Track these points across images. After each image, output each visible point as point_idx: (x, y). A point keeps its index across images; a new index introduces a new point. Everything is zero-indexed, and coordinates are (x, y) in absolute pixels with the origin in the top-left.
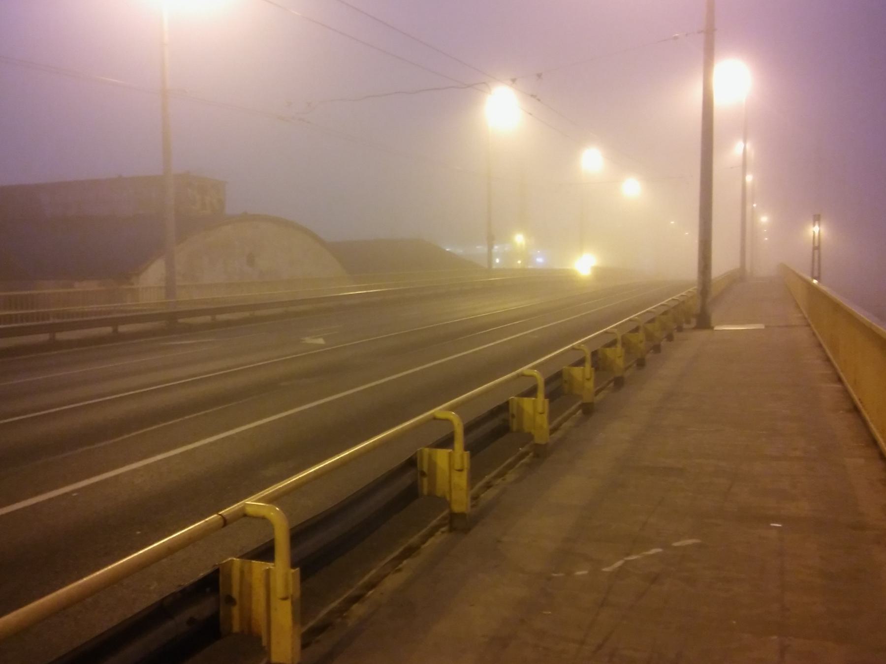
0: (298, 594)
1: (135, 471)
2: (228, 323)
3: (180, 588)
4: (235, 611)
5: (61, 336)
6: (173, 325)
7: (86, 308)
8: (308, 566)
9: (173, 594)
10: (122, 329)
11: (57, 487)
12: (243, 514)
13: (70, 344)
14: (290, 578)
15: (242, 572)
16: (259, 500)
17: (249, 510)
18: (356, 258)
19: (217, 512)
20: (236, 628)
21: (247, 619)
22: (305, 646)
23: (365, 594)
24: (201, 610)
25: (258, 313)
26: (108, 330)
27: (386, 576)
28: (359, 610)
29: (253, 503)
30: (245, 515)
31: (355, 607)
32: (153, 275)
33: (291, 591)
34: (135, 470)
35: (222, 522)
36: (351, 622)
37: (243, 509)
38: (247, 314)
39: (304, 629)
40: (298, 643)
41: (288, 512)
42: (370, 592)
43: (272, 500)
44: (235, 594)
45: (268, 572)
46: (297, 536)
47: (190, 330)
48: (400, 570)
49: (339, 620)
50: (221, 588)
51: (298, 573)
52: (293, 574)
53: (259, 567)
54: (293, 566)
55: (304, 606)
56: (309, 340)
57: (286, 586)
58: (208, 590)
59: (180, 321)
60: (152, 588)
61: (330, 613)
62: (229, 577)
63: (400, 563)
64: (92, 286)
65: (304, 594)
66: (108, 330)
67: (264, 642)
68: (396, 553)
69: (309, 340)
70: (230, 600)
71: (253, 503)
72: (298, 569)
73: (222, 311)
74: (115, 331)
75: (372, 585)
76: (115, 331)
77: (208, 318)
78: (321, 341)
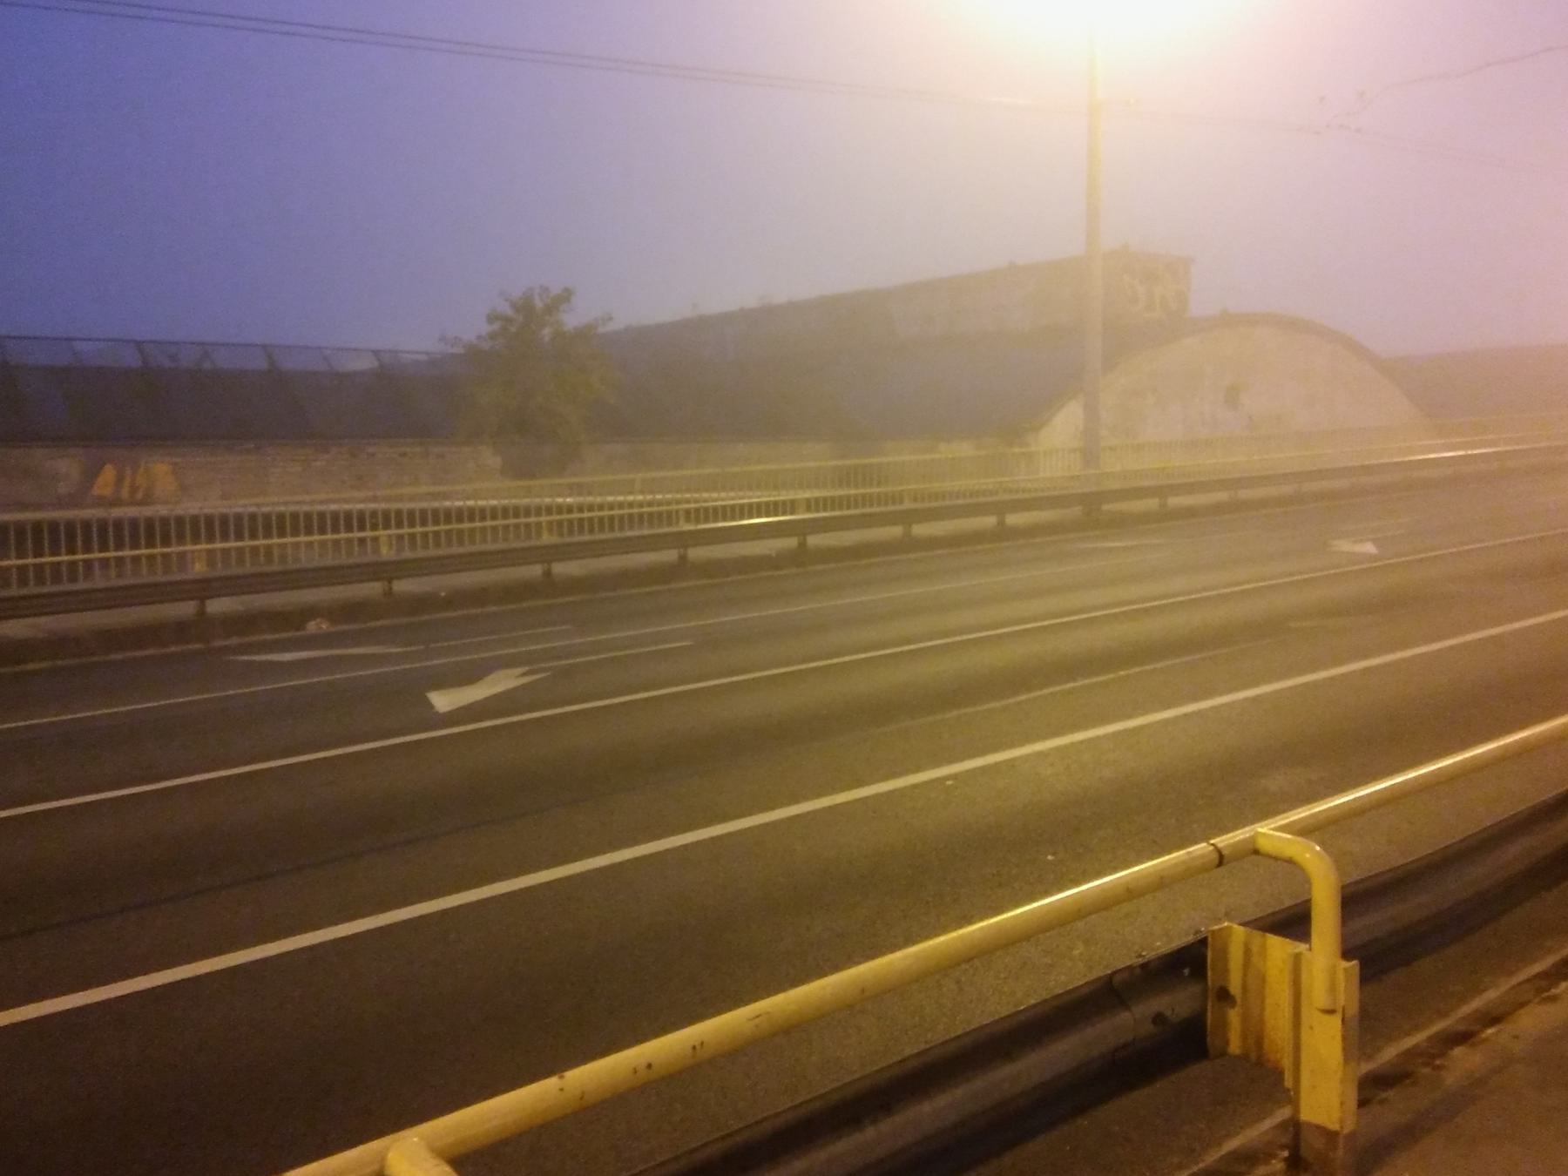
0: (1353, 1009)
1: (1046, 754)
2: (1191, 513)
3: (1141, 961)
4: (1234, 1016)
5: (920, 530)
6: (1092, 514)
7: (936, 486)
8: (1374, 958)
9: (1130, 968)
10: (1012, 519)
11: (918, 769)
12: (1252, 851)
13: (933, 543)
14: (1341, 976)
15: (1247, 952)
16: (1282, 829)
17: (1265, 845)
18: (1438, 387)
19: (1206, 839)
20: (1235, 1047)
21: (1256, 1034)
22: (1363, 1103)
23: (1481, 1031)
24: (1176, 1003)
25: (1245, 494)
26: (990, 521)
27: (1522, 1005)
28: (1464, 1060)
29: (1269, 832)
30: (1256, 852)
31: (1458, 1051)
32: (1062, 428)
33: (1342, 999)
34: (1040, 754)
35: (1215, 856)
36: (1451, 1079)
37: (1253, 839)
38: (1222, 496)
39: (1366, 1067)
40: (1352, 1097)
41: (1339, 860)
42: (1490, 1031)
43: (1304, 830)
44: (1235, 987)
45: (1297, 958)
46: (1353, 900)
47: (1122, 524)
48: (1554, 999)
49: (1426, 1070)
50: (1209, 973)
51: (1357, 969)
52: (1346, 970)
53: (1278, 948)
54: (1346, 954)
55: (1365, 1028)
56: (1345, 546)
57: (1332, 988)
58: (1186, 971)
59: (1105, 507)
60: (1076, 952)
61: (1410, 1054)
62: (1223, 954)
63: (1555, 984)
64: (964, 449)
65: (1365, 1014)
66: (990, 521)
67: (1288, 1082)
68: (1538, 968)
69: (1345, 546)
70: (1224, 995)
71: (1269, 832)
72: (1355, 962)
73: (1175, 489)
74: (1001, 523)
75: (1493, 1018)
76: (1001, 523)
77: (1152, 504)
78: (1370, 548)
